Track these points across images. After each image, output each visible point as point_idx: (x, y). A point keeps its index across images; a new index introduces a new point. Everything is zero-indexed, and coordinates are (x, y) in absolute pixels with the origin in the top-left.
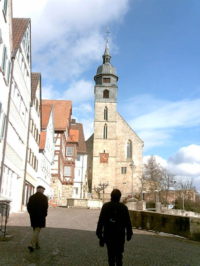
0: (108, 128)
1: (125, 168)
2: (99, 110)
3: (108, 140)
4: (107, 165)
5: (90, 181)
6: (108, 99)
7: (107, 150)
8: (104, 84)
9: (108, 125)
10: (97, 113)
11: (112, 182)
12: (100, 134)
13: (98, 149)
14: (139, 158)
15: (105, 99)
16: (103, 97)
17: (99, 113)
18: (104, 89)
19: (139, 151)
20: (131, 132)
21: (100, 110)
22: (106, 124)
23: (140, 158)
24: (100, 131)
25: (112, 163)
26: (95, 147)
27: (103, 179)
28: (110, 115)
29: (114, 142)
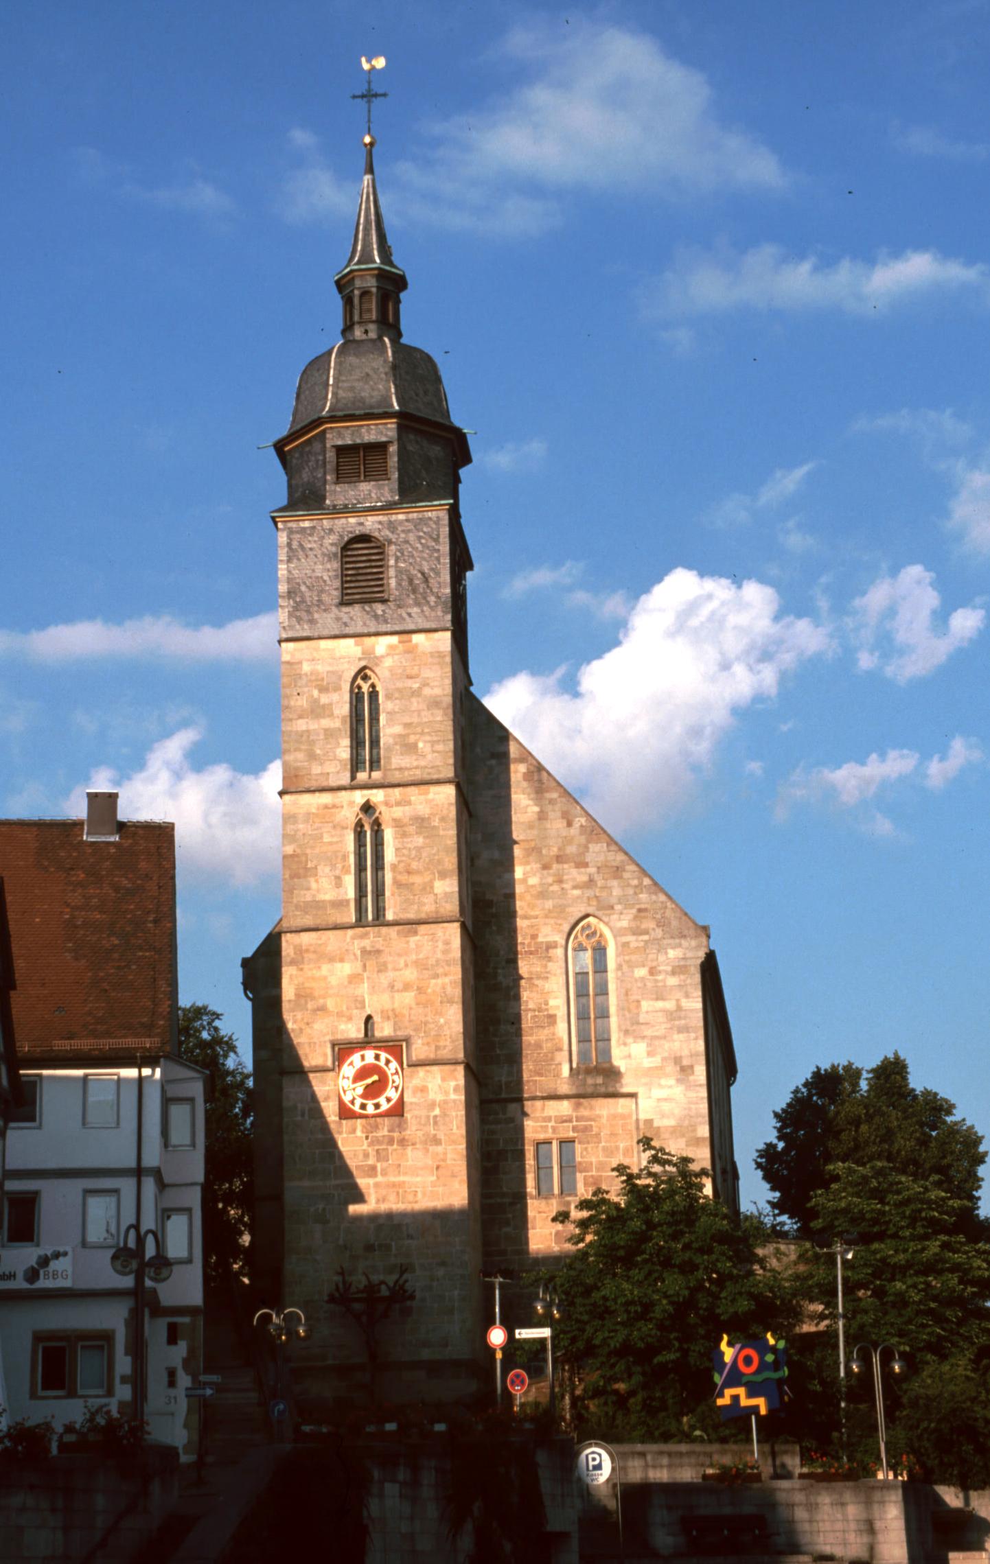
0: (389, 835)
1: (565, 1143)
2: (316, 701)
3: (393, 931)
4: (396, 1135)
5: (548, 1142)
6: (379, 608)
7: (392, 1015)
8: (337, 494)
9: (387, 815)
10: (301, 725)
11: (441, 1272)
12: (328, 895)
13: (322, 1009)
14: (677, 1060)
15: (356, 610)
16: (333, 593)
17: (313, 725)
18: (351, 524)
19: (670, 1005)
20: (598, 852)
21: (324, 699)
22: (367, 808)
23: (685, 1062)
24: (327, 869)
25: (437, 1112)
26: (298, 996)
27: (369, 1248)
28: (398, 729)
29: (447, 943)
